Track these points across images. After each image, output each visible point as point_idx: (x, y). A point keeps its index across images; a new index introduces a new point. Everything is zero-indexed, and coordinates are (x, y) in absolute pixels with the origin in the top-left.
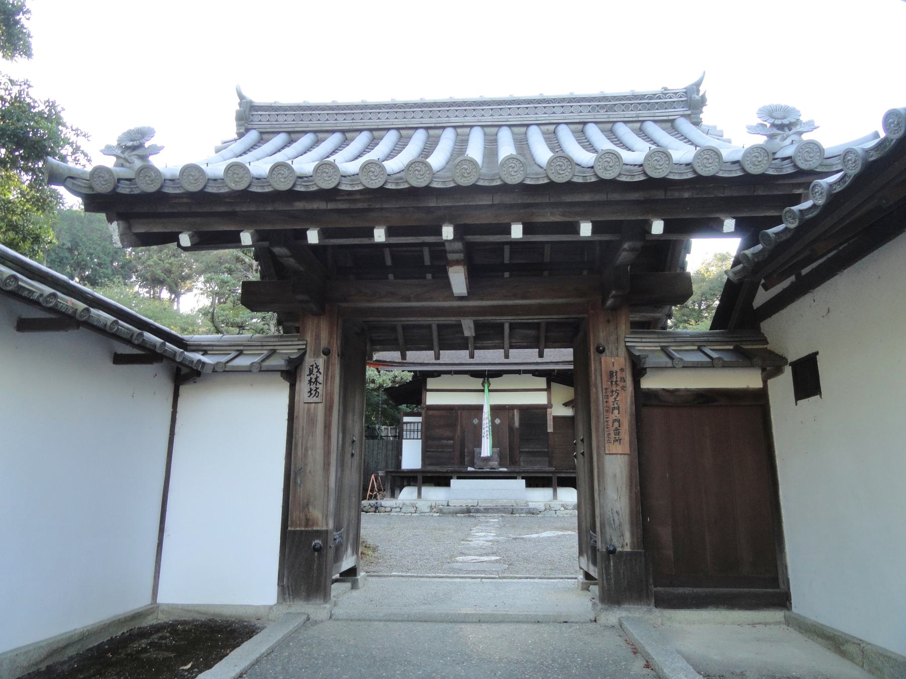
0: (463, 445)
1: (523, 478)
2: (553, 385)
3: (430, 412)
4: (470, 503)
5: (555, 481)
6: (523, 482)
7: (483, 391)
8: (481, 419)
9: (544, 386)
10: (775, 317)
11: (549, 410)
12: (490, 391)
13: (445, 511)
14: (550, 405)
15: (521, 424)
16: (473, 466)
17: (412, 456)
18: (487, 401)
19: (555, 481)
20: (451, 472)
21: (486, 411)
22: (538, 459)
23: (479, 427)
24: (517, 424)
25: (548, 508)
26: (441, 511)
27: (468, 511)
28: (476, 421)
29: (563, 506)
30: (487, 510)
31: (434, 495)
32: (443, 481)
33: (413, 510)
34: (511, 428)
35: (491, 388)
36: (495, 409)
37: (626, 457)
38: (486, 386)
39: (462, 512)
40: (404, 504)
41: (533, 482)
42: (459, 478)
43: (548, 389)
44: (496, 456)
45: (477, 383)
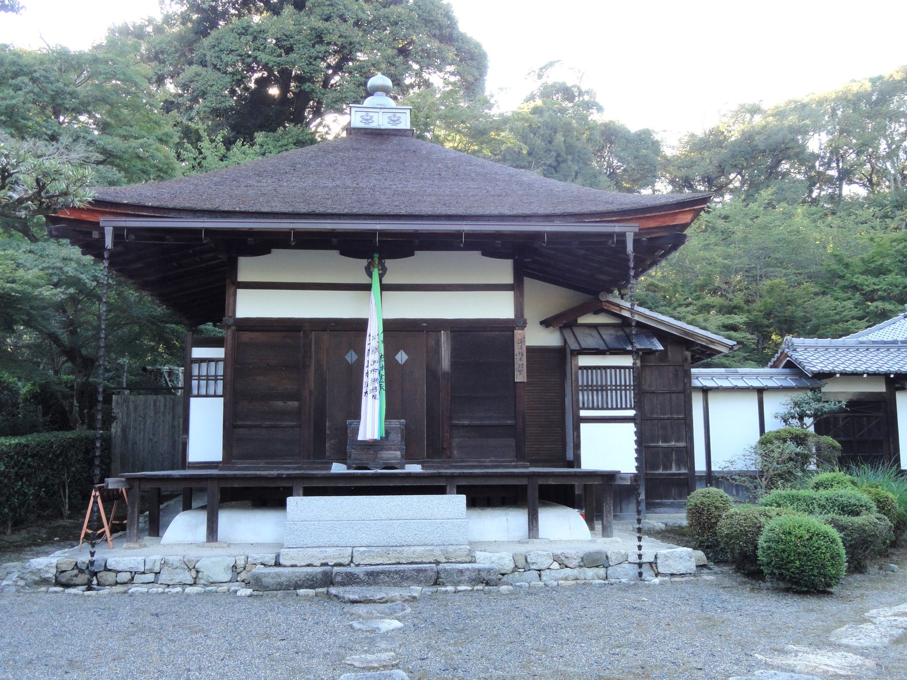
0: (321, 413)
1: (460, 490)
2: (527, 281)
3: (246, 336)
4: (332, 555)
5: (533, 493)
6: (463, 498)
7: (367, 287)
8: (361, 352)
9: (508, 278)
10: (562, 310)
11: (518, 333)
12: (384, 288)
13: (267, 581)
14: (519, 322)
15: (453, 364)
16: (343, 460)
17: (206, 435)
18: (376, 310)
19: (533, 493)
20: (290, 478)
21: (375, 331)
22: (492, 442)
23: (356, 373)
24: (446, 363)
25: (523, 565)
26: (256, 583)
27: (326, 580)
28: (351, 357)
29: (556, 559)
30: (374, 577)
31: (250, 531)
32: (269, 497)
33: (188, 577)
34: (432, 374)
35: (387, 280)
36: (392, 328)
37: (631, 428)
38: (376, 273)
39: (311, 583)
40: (165, 563)
41: (482, 497)
42: (309, 492)
43: (517, 287)
44: (396, 437)
45: (353, 270)
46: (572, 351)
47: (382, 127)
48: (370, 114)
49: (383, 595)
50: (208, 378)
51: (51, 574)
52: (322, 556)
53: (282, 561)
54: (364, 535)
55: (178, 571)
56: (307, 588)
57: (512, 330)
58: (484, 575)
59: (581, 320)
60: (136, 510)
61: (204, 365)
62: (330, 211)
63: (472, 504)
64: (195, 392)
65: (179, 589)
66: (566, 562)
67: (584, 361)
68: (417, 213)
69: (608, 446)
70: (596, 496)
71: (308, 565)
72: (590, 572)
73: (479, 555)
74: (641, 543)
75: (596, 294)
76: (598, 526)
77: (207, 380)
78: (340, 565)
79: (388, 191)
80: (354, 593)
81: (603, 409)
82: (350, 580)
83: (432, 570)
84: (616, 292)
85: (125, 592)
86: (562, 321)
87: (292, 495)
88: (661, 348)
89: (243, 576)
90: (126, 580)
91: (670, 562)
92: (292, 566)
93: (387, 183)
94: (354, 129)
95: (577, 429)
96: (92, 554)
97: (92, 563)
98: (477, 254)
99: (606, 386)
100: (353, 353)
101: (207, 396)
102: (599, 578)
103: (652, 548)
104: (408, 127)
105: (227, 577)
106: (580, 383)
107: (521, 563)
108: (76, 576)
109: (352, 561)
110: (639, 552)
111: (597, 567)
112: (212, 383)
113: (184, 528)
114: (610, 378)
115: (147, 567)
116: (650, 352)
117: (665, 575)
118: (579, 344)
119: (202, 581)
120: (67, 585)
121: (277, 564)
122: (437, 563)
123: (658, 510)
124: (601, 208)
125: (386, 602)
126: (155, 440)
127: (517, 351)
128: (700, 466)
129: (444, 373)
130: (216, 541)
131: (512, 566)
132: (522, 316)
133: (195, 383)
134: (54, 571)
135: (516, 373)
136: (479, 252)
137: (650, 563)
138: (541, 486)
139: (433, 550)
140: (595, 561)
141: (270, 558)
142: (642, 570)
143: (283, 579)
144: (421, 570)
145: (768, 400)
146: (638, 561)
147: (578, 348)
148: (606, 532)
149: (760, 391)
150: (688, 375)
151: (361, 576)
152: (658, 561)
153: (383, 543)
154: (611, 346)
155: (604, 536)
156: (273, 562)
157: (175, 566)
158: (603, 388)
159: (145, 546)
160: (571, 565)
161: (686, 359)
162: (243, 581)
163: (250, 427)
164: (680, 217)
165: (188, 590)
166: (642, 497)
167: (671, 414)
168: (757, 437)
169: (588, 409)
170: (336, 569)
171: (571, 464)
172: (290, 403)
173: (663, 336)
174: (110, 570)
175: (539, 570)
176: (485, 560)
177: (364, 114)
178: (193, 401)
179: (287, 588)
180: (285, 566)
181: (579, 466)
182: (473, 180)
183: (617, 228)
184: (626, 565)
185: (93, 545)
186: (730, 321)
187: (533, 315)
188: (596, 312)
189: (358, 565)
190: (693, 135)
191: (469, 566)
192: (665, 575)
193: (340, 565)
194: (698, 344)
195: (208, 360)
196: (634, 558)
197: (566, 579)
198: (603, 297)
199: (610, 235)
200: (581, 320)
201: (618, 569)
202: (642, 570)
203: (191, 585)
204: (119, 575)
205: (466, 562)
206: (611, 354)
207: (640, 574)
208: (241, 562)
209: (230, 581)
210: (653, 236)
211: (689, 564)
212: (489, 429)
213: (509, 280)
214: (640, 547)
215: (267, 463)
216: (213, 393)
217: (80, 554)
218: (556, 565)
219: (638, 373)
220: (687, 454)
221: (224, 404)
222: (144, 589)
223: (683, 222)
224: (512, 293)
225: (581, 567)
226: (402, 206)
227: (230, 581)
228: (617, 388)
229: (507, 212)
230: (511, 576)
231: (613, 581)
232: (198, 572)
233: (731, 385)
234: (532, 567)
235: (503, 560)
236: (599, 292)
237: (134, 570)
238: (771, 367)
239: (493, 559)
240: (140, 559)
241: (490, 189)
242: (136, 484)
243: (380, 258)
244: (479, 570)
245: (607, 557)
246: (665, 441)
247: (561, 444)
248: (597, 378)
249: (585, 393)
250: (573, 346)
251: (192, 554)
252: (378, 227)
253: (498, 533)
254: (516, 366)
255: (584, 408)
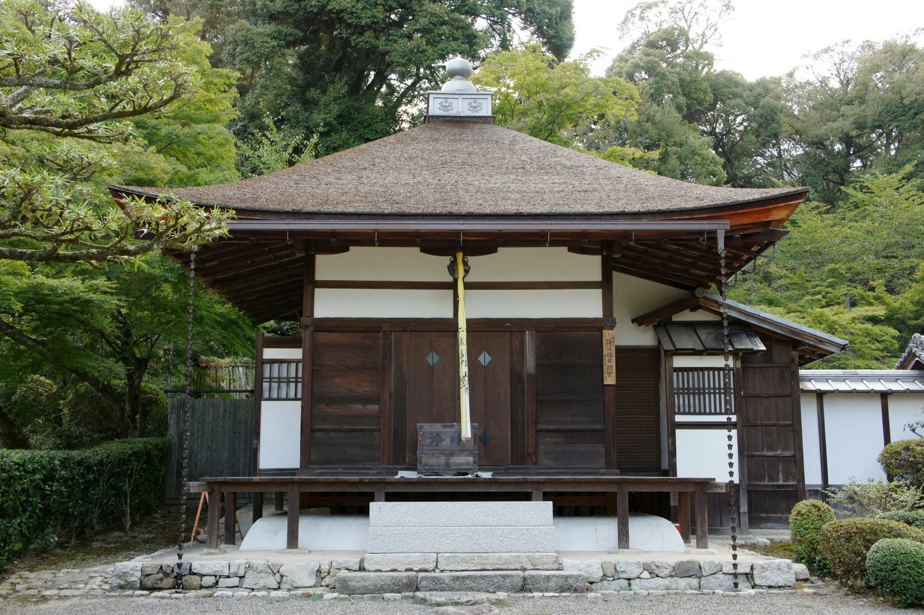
1: (546, 497)
3: (324, 337)
4: (417, 560)
5: (623, 503)
6: (549, 505)
14: (608, 321)
15: (538, 366)
17: (280, 439)
20: (372, 483)
22: (581, 447)
25: (611, 575)
29: (646, 567)
30: (461, 583)
31: (331, 540)
32: (352, 504)
33: (272, 581)
35: (470, 278)
40: (249, 567)
41: (569, 506)
42: (391, 497)
45: (435, 267)
46: (666, 351)
47: (462, 114)
48: (449, 100)
49: (470, 598)
50: (279, 380)
51: (136, 578)
52: (407, 561)
53: (366, 566)
54: (449, 541)
55: (263, 575)
56: (392, 592)
57: (601, 330)
58: (571, 581)
59: (677, 318)
60: (216, 513)
61: (276, 366)
62: (413, 211)
63: (559, 512)
64: (266, 395)
65: (264, 593)
66: (657, 572)
67: (679, 362)
68: (502, 212)
69: (706, 454)
70: (696, 509)
71: (393, 571)
72: (683, 582)
73: (566, 561)
74: (736, 552)
75: (692, 289)
76: (693, 541)
77: (279, 382)
78: (426, 571)
79: (471, 188)
80: (441, 596)
81: (700, 413)
82: (438, 585)
83: (518, 576)
84: (714, 286)
85: (211, 596)
86: (656, 318)
87: (373, 501)
88: (763, 348)
89: (328, 580)
90: (211, 584)
91: (767, 573)
92: (376, 571)
93: (470, 178)
94: (432, 116)
95: (673, 435)
96: (180, 557)
97: (179, 566)
98: (564, 249)
99: (704, 388)
100: (435, 356)
101: (278, 399)
102: (691, 589)
103: (746, 559)
104: (490, 114)
105: (312, 581)
106: (675, 386)
107: (610, 571)
108: (161, 579)
109: (437, 567)
110: (734, 562)
111: (690, 577)
112: (284, 385)
113: (263, 537)
114: (709, 381)
115: (231, 571)
116: (753, 352)
117: (761, 587)
118: (674, 345)
119: (287, 586)
120: (152, 589)
121: (362, 569)
122: (524, 570)
123: (763, 525)
124: (690, 205)
125: (474, 604)
126: (214, 447)
127: (605, 352)
128: (812, 477)
129: (529, 376)
130: (296, 547)
131: (602, 574)
132: (611, 315)
133: (266, 385)
134: (139, 574)
135: (605, 375)
136: (566, 248)
137: (746, 574)
138: (630, 493)
139: (519, 557)
140: (687, 571)
141: (354, 562)
142: (737, 581)
143: (369, 582)
144: (508, 576)
145: (894, 408)
146: (733, 571)
147: (672, 348)
148: (702, 544)
149: (885, 396)
150: (797, 379)
151: (447, 581)
152: (755, 572)
153: (469, 549)
154: (707, 346)
155: (698, 547)
156: (357, 567)
157: (259, 570)
158: (700, 391)
159: (225, 552)
160: (662, 575)
161: (793, 360)
162: (327, 586)
163: (327, 431)
164: (774, 212)
165: (274, 594)
166: (744, 508)
167: (777, 419)
168: (879, 446)
169: (684, 413)
170: (421, 574)
171: (666, 473)
172: (370, 406)
173: (766, 336)
174: (195, 574)
175: (629, 579)
176: (572, 567)
177: (443, 100)
178: (264, 404)
179: (372, 592)
180: (369, 571)
181: (676, 475)
182: (558, 174)
183: (705, 226)
184: (720, 576)
185: (181, 548)
186: (870, 314)
187: (622, 316)
188: (694, 309)
189: (442, 571)
190: (869, 46)
191: (557, 573)
192: (761, 587)
193: (426, 571)
194: (805, 344)
195: (280, 362)
196: (729, 569)
197: (657, 588)
198: (699, 292)
199: (701, 233)
200: (677, 318)
201: (711, 579)
202: (737, 581)
203: (275, 589)
204: (204, 578)
205: (553, 570)
206: (708, 354)
207: (736, 585)
208: (325, 568)
209: (315, 586)
210: (746, 232)
211: (788, 576)
212: (576, 428)
213: (596, 275)
214: (735, 557)
215: (346, 469)
216: (284, 396)
217: (168, 559)
218: (646, 574)
219: (741, 376)
220: (797, 462)
221: (302, 407)
222: (229, 593)
223: (778, 218)
224: (600, 290)
225: (671, 576)
226: (486, 205)
227: (315, 586)
228: (715, 391)
229: (592, 209)
230: (600, 584)
231: (706, 591)
232: (282, 576)
233: (866, 388)
234: (621, 576)
235: (591, 566)
236: (695, 288)
237: (218, 574)
238: (898, 368)
239: (581, 567)
240: (225, 563)
241: (577, 183)
242: (216, 488)
243: (465, 255)
244: (567, 577)
245: (700, 567)
246: (769, 449)
247: (655, 453)
248: (693, 381)
249: (681, 396)
250: (667, 346)
251: (275, 559)
252: (462, 227)
253: (588, 544)
254: (605, 368)
255: (679, 413)
